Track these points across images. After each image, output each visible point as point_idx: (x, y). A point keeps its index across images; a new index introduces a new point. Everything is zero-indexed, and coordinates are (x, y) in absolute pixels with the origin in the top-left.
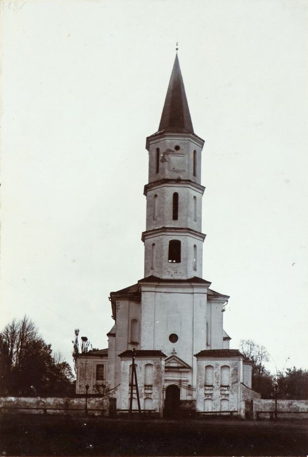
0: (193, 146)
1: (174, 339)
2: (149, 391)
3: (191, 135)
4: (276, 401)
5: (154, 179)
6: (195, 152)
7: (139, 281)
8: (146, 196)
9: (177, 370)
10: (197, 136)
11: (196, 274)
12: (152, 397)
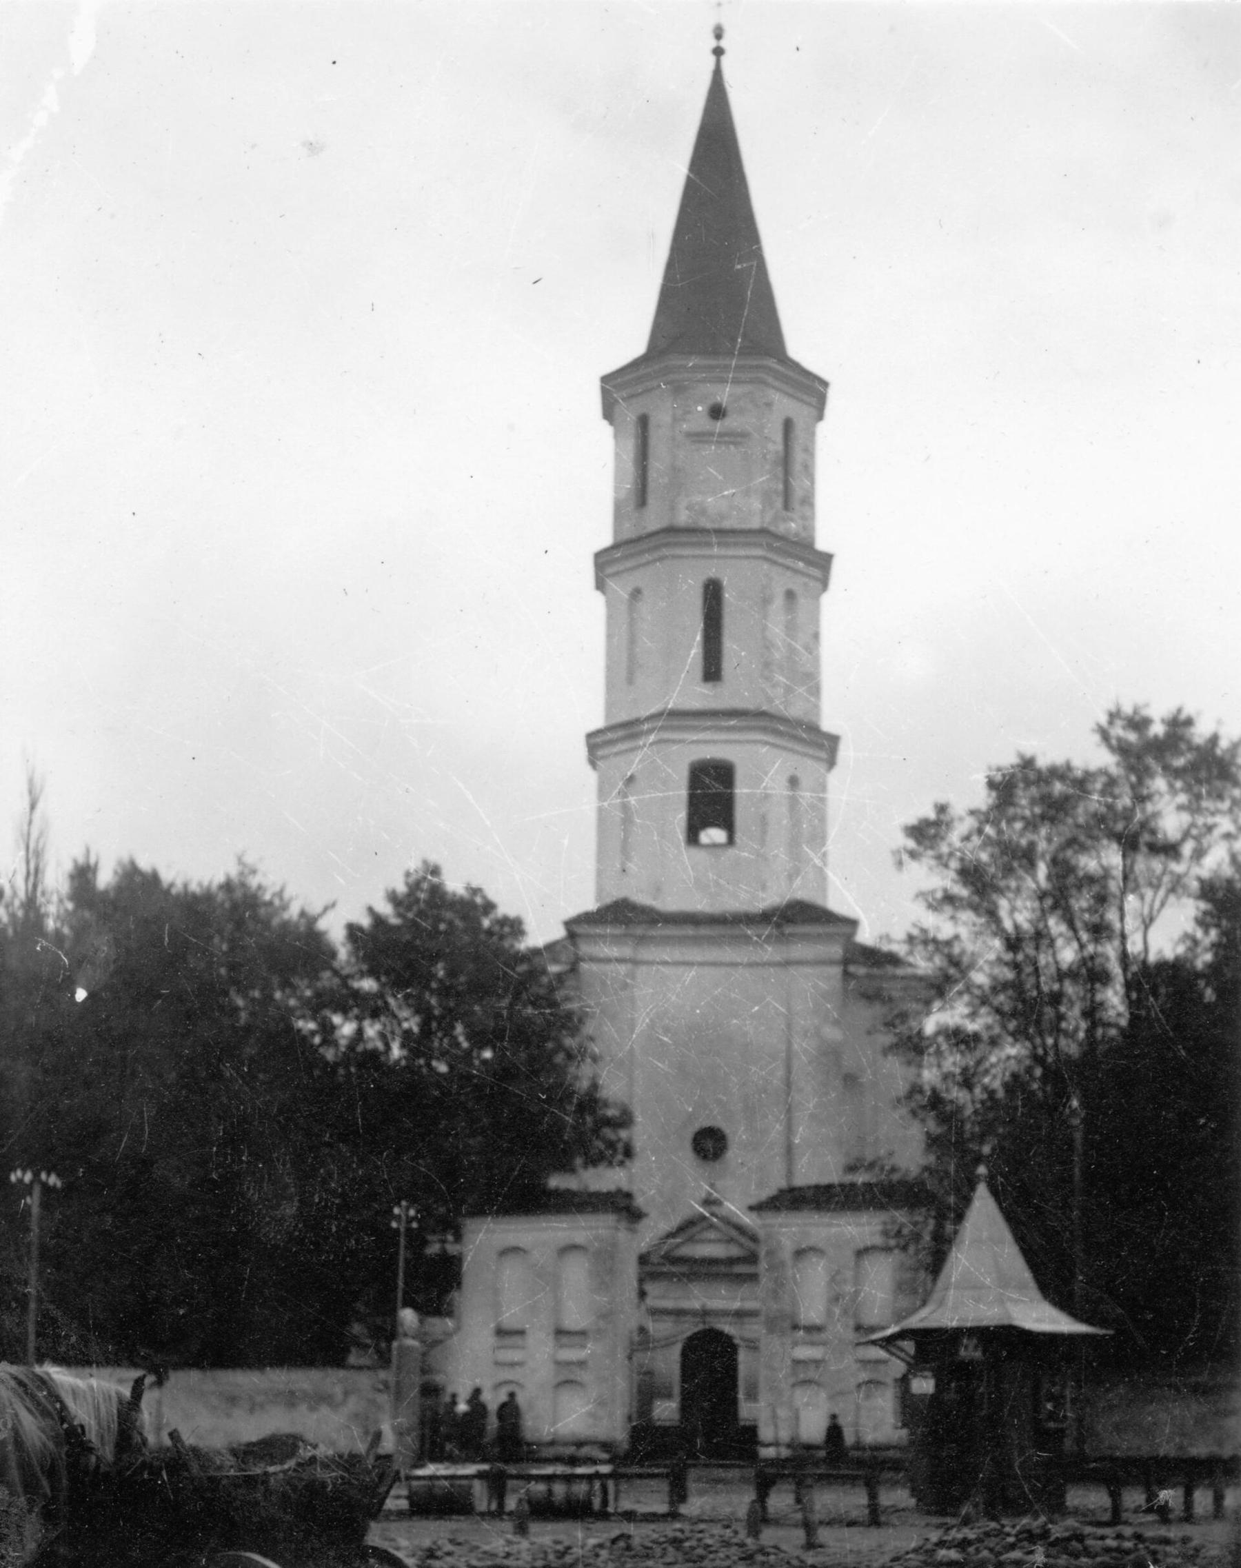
0: (784, 405)
1: (709, 1144)
2: (515, 1356)
3: (772, 363)
4: (873, 1496)
5: (629, 532)
6: (788, 425)
7: (569, 924)
8: (604, 592)
9: (723, 1269)
10: (796, 366)
11: (801, 891)
12: (585, 1376)
